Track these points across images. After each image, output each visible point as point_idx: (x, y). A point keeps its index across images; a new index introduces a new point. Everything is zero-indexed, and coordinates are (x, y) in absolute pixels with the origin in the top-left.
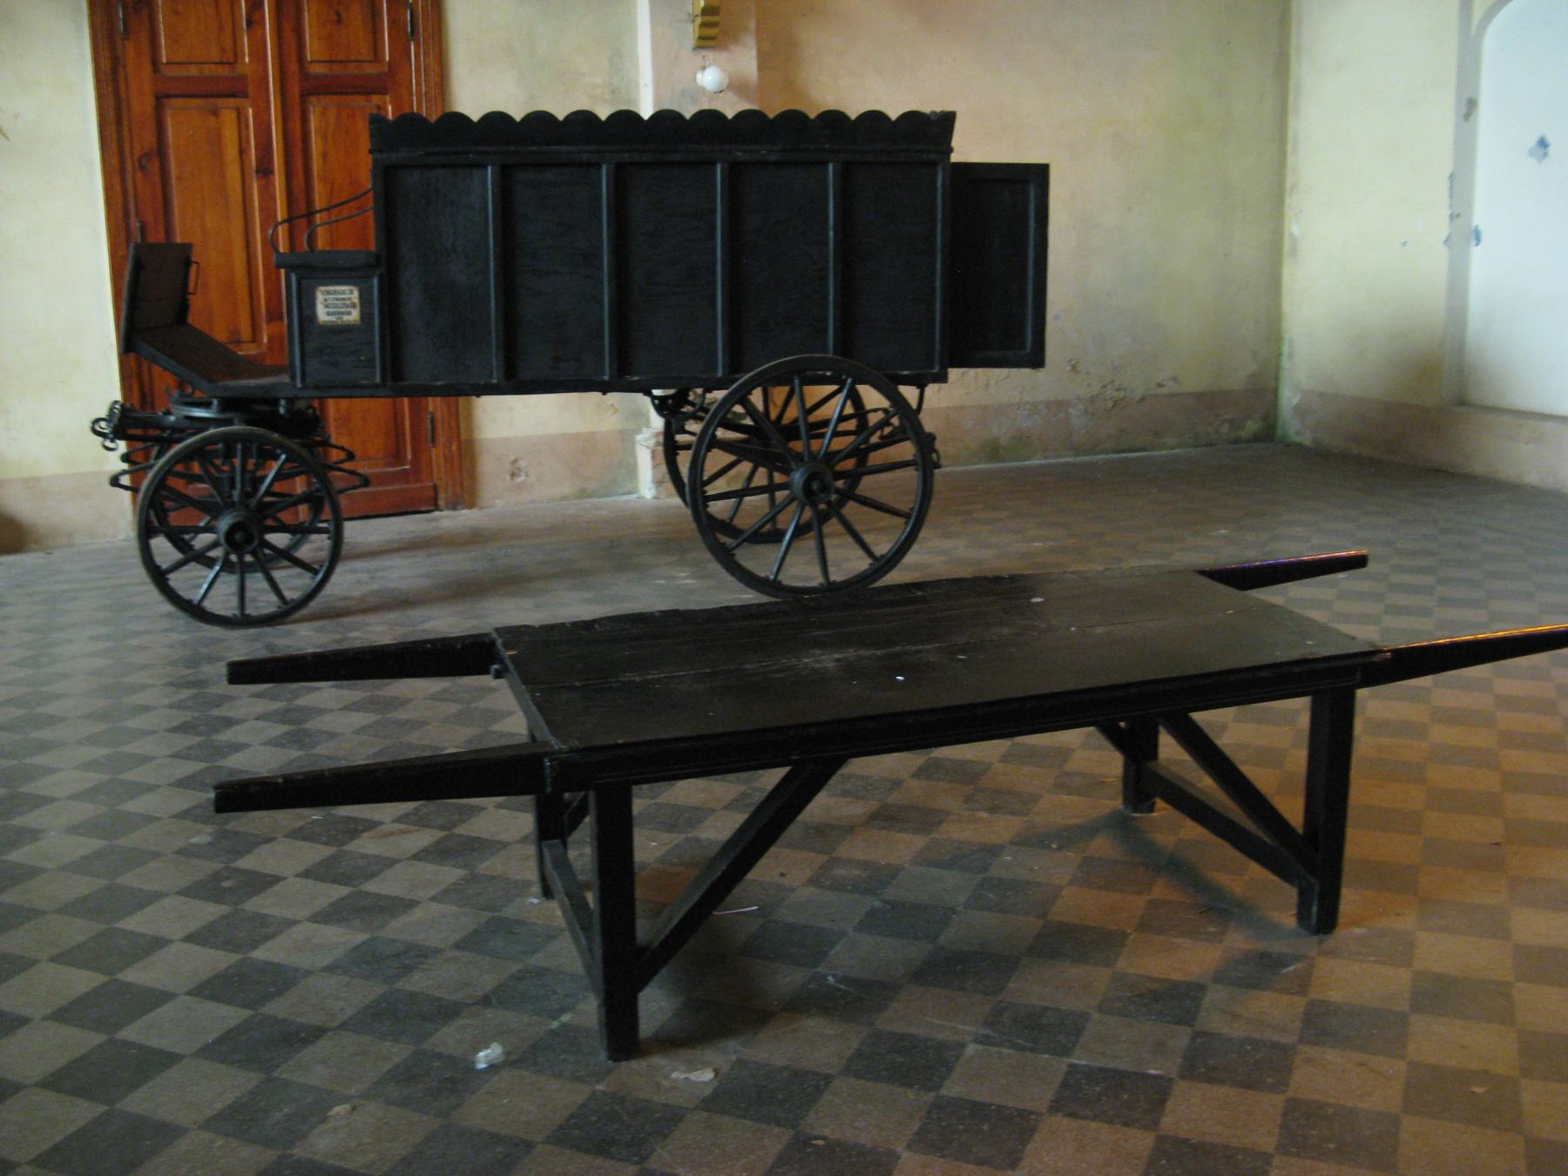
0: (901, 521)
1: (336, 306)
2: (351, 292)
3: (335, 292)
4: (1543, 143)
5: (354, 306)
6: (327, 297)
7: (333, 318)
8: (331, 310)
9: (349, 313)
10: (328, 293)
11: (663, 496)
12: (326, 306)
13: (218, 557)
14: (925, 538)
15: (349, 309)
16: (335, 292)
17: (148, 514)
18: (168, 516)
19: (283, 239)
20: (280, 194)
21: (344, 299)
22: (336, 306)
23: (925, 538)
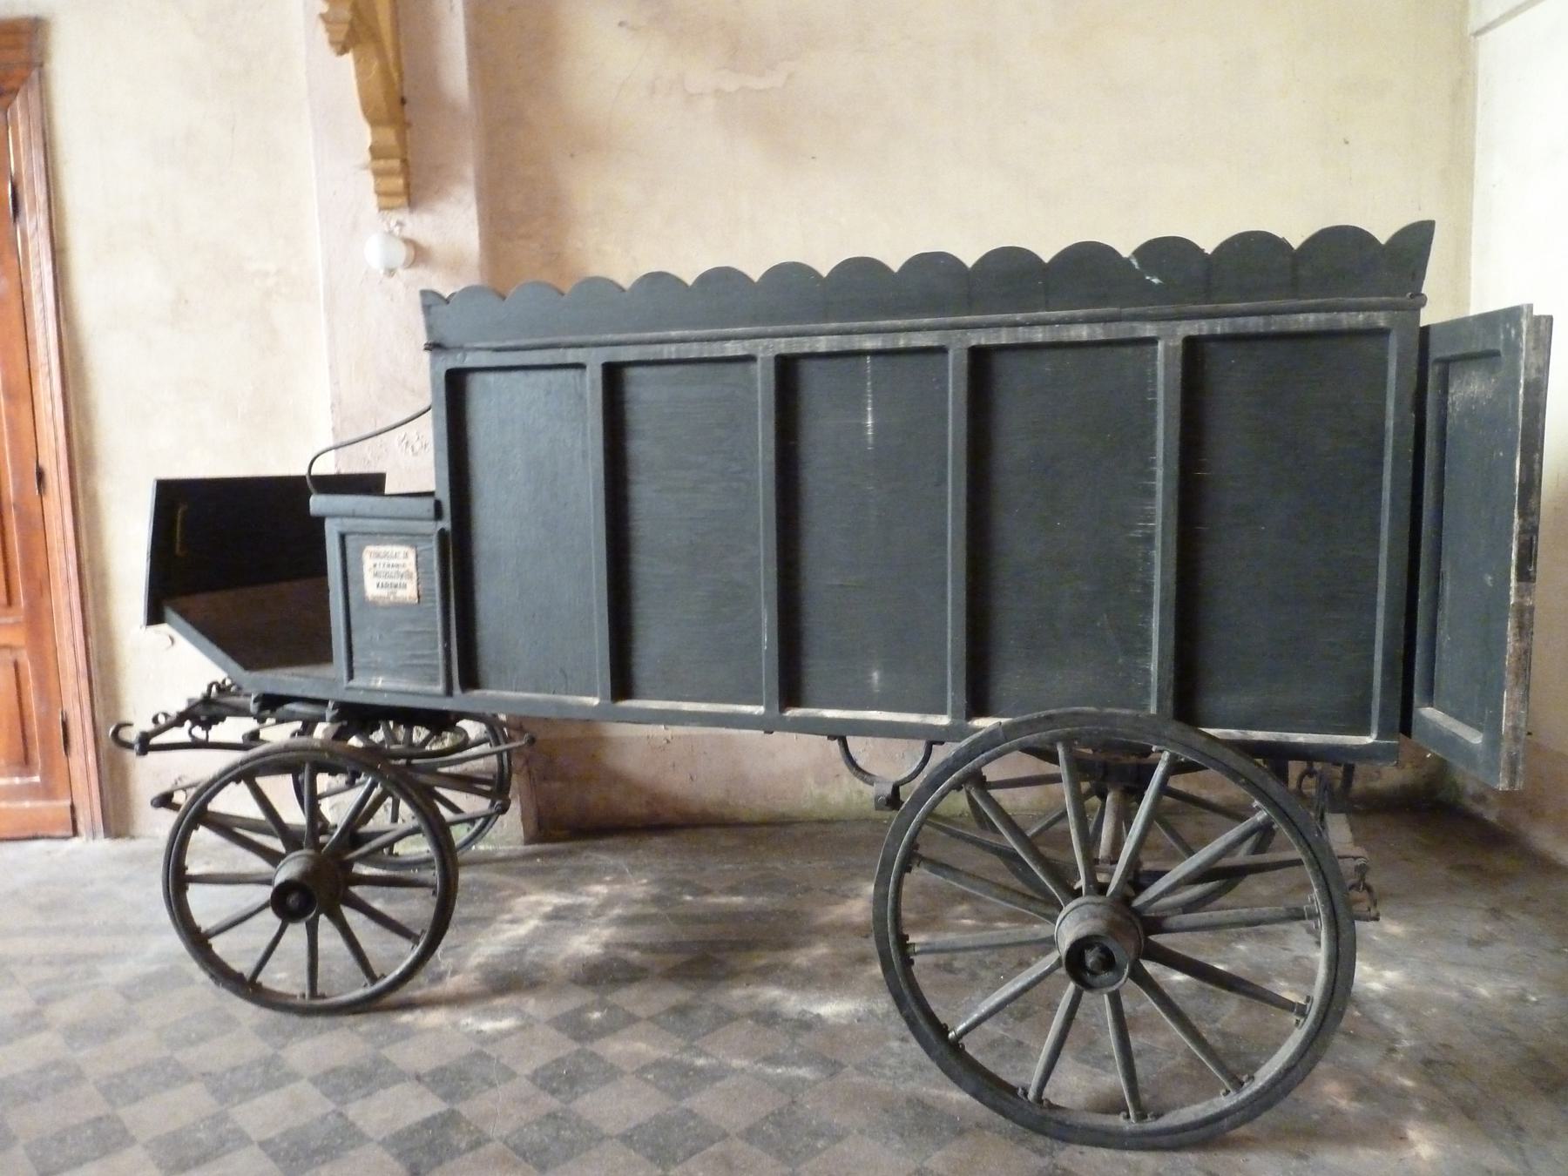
0: (430, 891)
1: (387, 575)
2: (406, 556)
3: (386, 555)
4: (1347, 143)
5: (410, 576)
6: (378, 561)
7: (384, 592)
8: (382, 580)
9: (405, 586)
10: (378, 556)
11: (470, 827)
12: (376, 575)
13: (1269, 817)
14: (467, 921)
15: (404, 581)
16: (386, 555)
17: (479, 818)
18: (197, 829)
19: (955, 667)
20: (954, 635)
21: (398, 566)
22: (387, 575)
23: (467, 921)
